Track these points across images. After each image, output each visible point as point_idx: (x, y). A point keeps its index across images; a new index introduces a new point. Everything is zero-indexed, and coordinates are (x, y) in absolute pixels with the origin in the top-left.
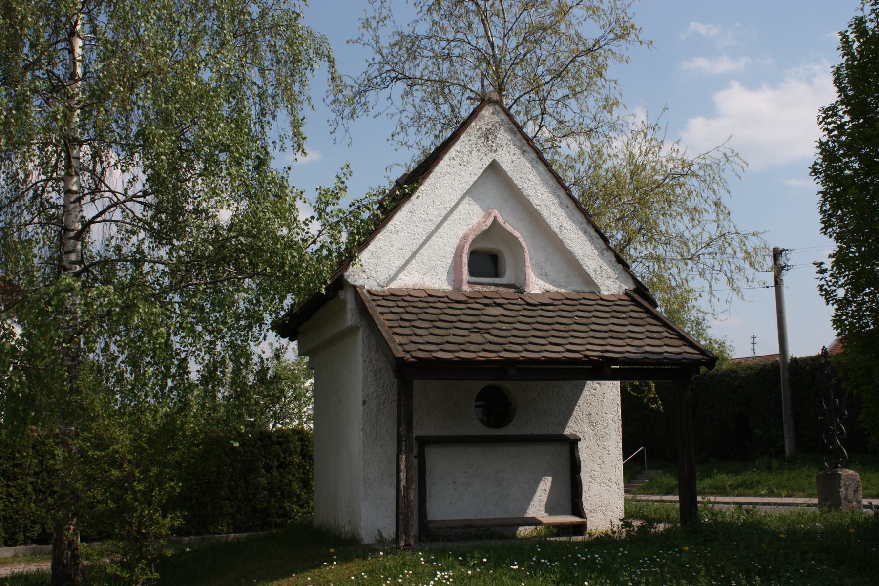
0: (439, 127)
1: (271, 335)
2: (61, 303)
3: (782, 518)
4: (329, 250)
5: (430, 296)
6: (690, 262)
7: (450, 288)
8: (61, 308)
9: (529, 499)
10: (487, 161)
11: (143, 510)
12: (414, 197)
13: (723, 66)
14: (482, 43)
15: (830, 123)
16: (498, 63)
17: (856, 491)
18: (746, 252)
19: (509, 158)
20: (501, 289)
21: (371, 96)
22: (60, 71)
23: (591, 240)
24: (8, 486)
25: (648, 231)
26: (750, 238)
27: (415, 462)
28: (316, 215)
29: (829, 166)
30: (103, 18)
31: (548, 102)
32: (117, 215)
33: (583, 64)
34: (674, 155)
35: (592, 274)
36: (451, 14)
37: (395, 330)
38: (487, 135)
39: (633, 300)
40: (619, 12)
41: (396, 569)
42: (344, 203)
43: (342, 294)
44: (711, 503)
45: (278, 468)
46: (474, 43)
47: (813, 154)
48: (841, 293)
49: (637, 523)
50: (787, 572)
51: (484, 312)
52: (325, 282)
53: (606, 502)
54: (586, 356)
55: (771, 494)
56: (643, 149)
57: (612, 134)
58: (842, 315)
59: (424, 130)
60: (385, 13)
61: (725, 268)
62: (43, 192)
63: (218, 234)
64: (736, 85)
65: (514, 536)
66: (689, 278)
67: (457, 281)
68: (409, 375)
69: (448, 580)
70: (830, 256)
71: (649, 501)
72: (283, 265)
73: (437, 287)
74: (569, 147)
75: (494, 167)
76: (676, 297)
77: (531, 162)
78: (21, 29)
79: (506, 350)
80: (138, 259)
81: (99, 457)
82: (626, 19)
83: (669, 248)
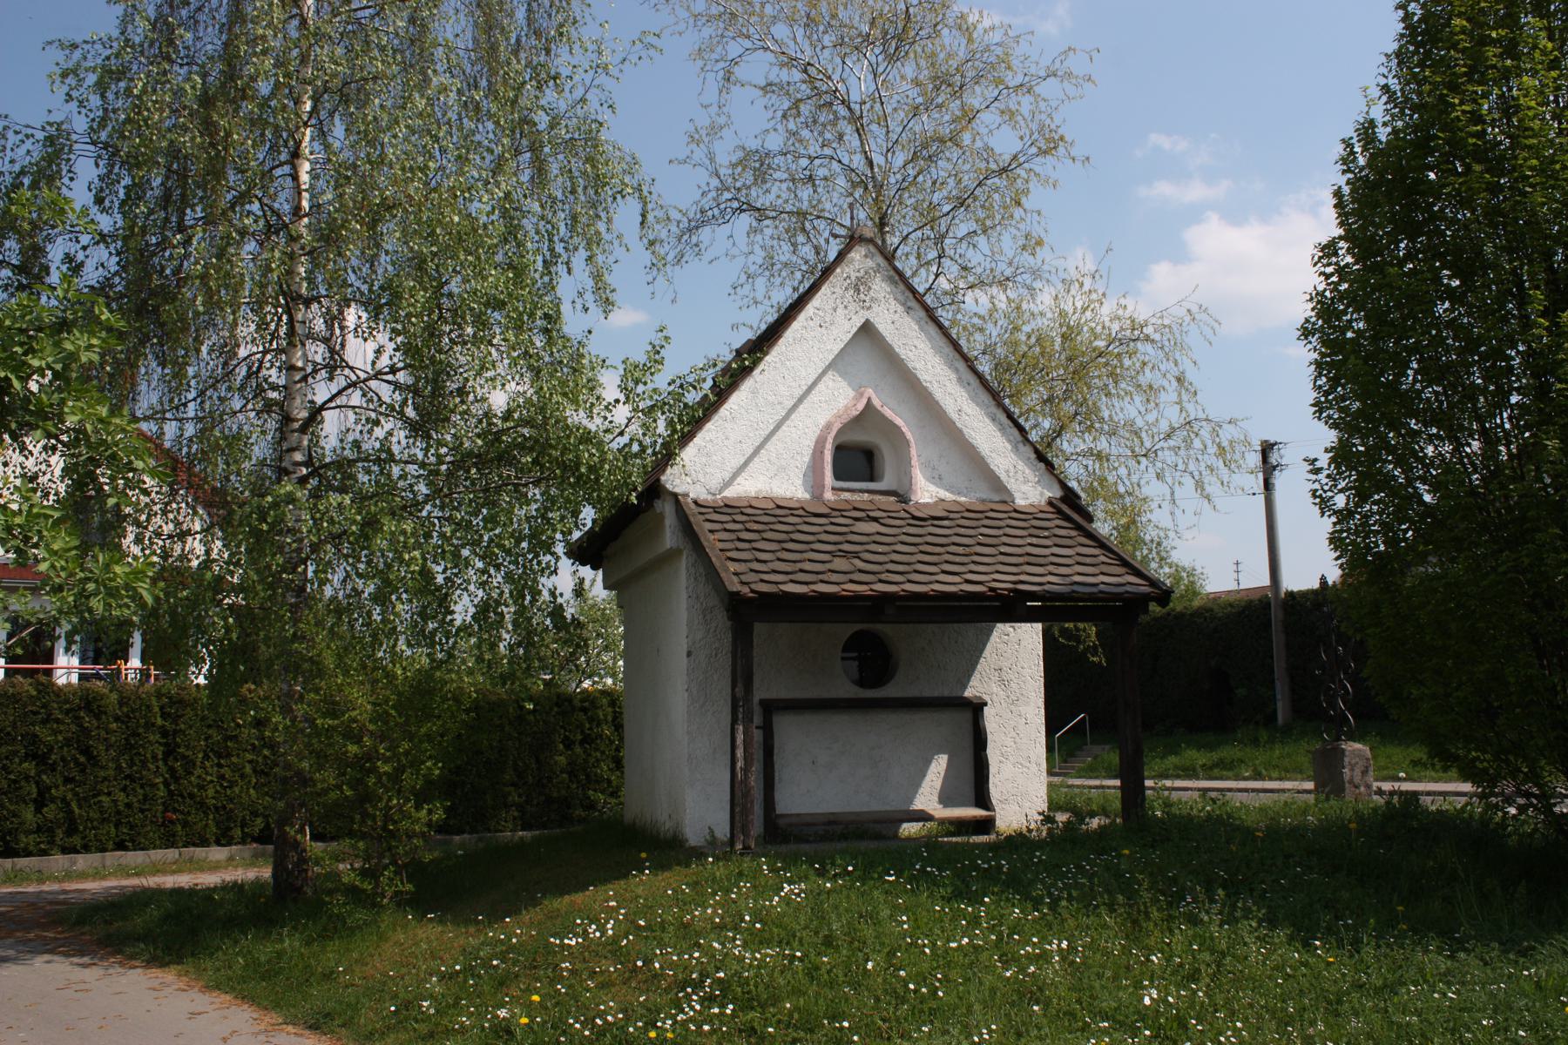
0: (798, 275)
1: (566, 565)
2: (280, 519)
3: (1263, 810)
4: (641, 444)
5: (779, 507)
6: (1143, 460)
7: (807, 496)
8: (278, 527)
9: (917, 785)
10: (858, 322)
11: (390, 799)
12: (756, 372)
13: (1196, 192)
14: (858, 161)
15: (1329, 265)
16: (879, 187)
17: (1365, 772)
18: (1219, 445)
19: (889, 317)
20: (877, 497)
21: (705, 234)
22: (283, 205)
23: (1002, 429)
24: (220, 766)
25: (1088, 418)
26: (1225, 426)
27: (758, 735)
28: (622, 398)
29: (1326, 322)
30: (338, 130)
31: (947, 241)
32: (356, 398)
33: (997, 190)
34: (1120, 312)
35: (1003, 477)
36: (815, 122)
37: (729, 554)
38: (858, 286)
39: (1059, 511)
40: (1043, 117)
41: (729, 880)
42: (661, 381)
43: (658, 504)
44: (1168, 789)
45: (582, 743)
46: (846, 161)
47: (1304, 310)
48: (1340, 501)
49: (1061, 818)
50: (1263, 882)
51: (854, 529)
52: (635, 489)
53: (1022, 788)
54: (991, 589)
55: (1258, 776)
56: (1079, 304)
57: (1038, 285)
58: (1342, 531)
59: (778, 281)
60: (722, 120)
61: (1192, 467)
62: (260, 368)
63: (490, 424)
64: (1214, 219)
65: (896, 836)
66: (1142, 482)
67: (816, 486)
68: (747, 614)
69: (798, 895)
70: (1326, 451)
71: (1084, 787)
72: (578, 465)
73: (789, 495)
74: (976, 302)
75: (867, 329)
76: (1124, 509)
77: (918, 322)
78: (225, 149)
79: (881, 581)
80: (385, 456)
81: (332, 728)
82: (1053, 126)
83: (1114, 440)
